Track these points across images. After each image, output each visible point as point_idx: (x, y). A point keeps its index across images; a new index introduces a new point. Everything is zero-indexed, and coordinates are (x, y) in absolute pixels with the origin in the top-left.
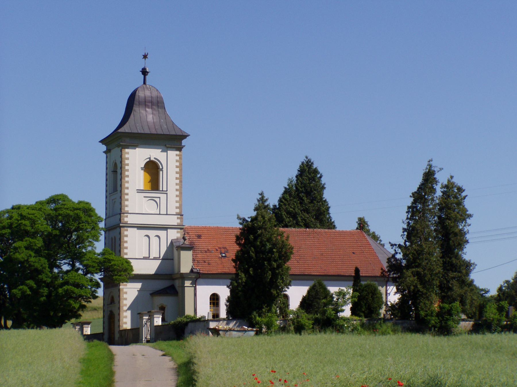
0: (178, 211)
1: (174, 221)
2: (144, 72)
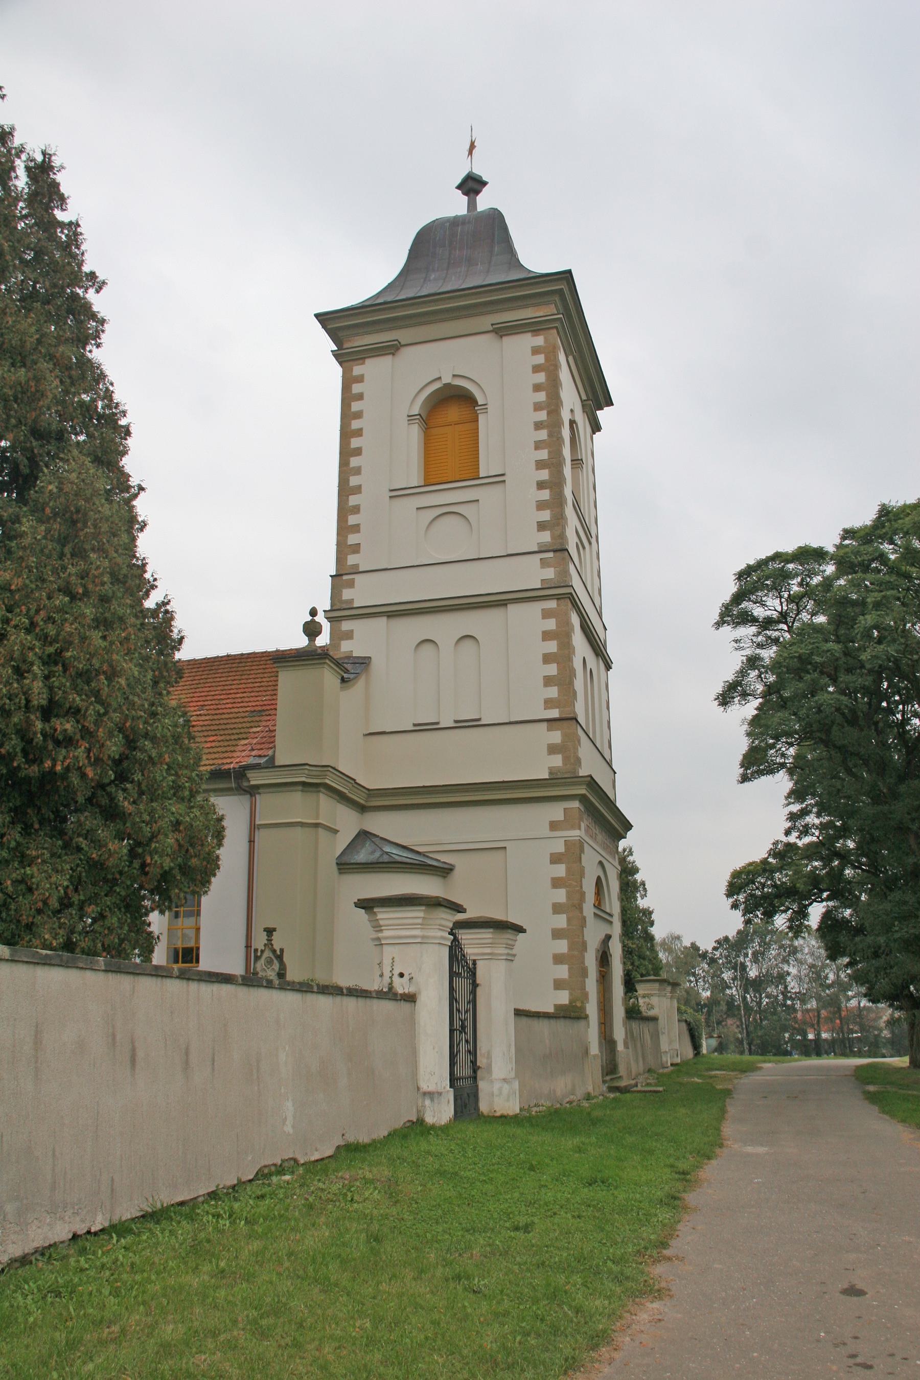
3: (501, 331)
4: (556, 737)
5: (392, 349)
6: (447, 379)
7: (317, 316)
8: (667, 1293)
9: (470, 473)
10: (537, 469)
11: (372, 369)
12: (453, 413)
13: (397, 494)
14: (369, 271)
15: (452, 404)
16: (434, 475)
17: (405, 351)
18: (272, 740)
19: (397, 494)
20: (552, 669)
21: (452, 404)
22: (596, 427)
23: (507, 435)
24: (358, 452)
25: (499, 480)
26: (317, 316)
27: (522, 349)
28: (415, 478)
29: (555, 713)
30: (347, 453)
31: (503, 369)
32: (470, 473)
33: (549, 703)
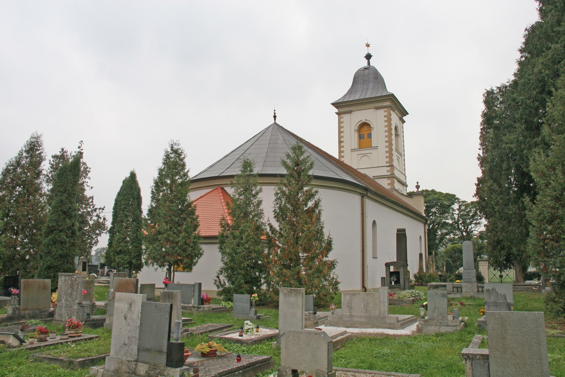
2: (368, 57)
3: (377, 108)
4: (389, 168)
5: (350, 112)
6: (363, 121)
7: (333, 104)
8: (288, 161)
9: (370, 146)
10: (398, 230)
11: (346, 117)
12: (365, 128)
13: (353, 150)
14: (341, 88)
15: (364, 126)
16: (361, 147)
17: (354, 113)
18: (392, 306)
19: (353, 150)
20: (387, 155)
21: (364, 126)
22: (404, 122)
23: (379, 136)
24: (343, 132)
25: (376, 147)
26: (333, 104)
27: (382, 113)
28: (356, 146)
29: (388, 165)
30: (340, 132)
31: (376, 118)
32: (370, 146)
33: (387, 162)
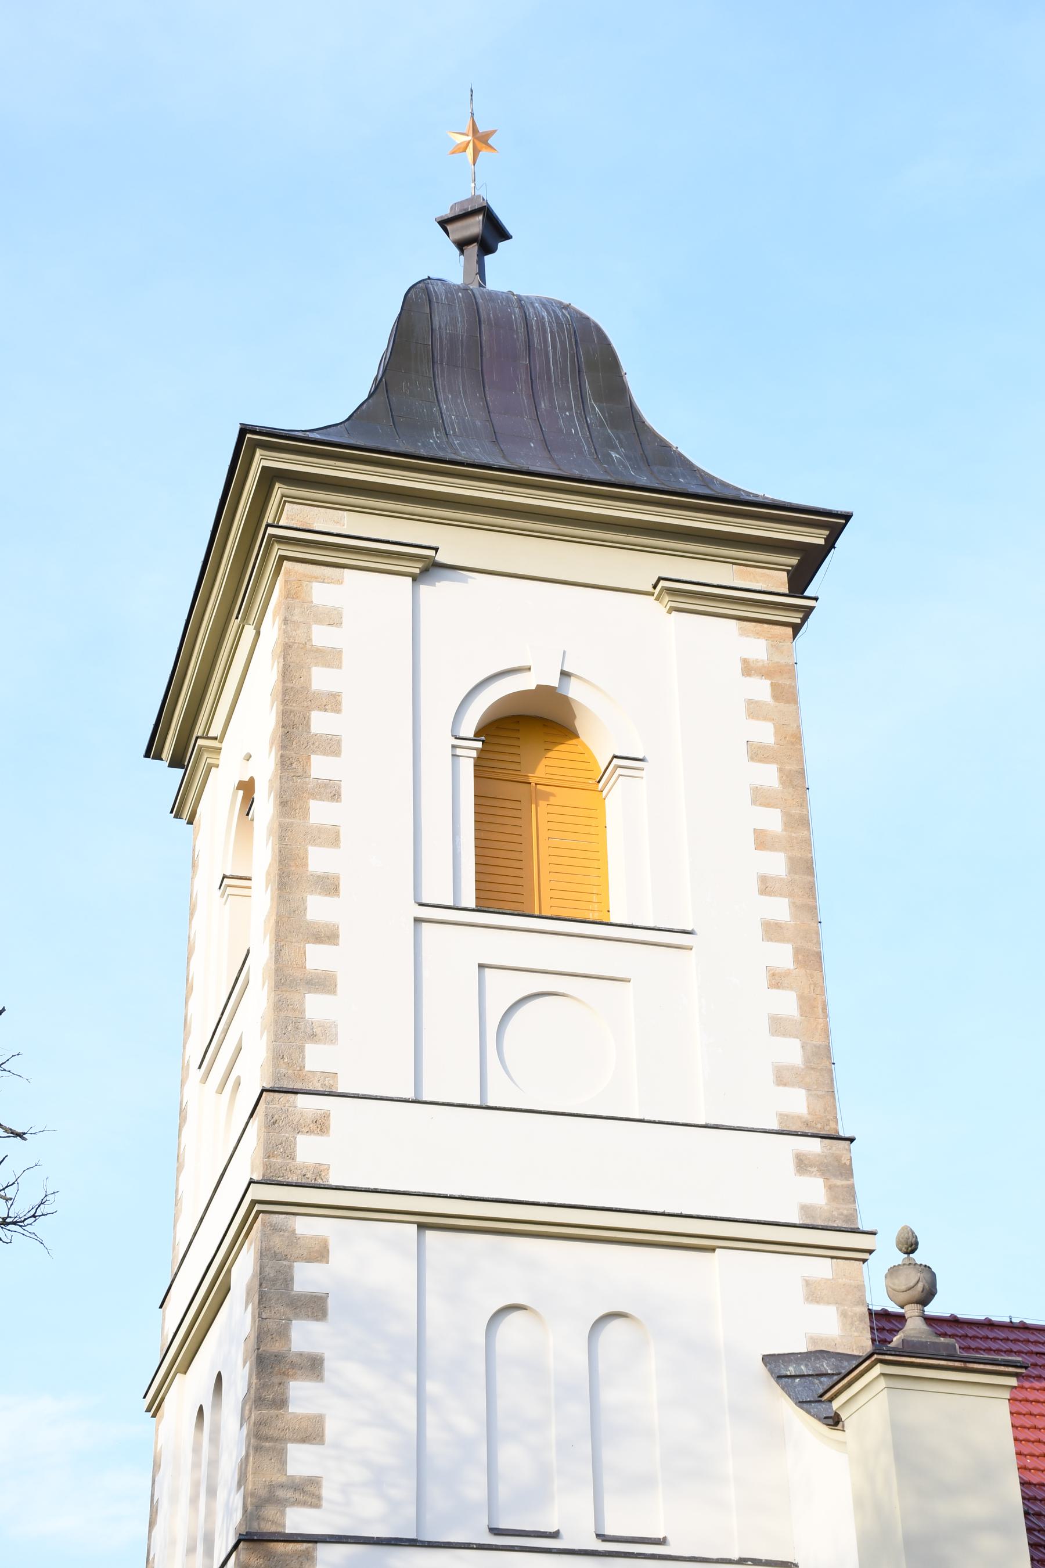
0: (797, 1103)
1: (779, 1186)
